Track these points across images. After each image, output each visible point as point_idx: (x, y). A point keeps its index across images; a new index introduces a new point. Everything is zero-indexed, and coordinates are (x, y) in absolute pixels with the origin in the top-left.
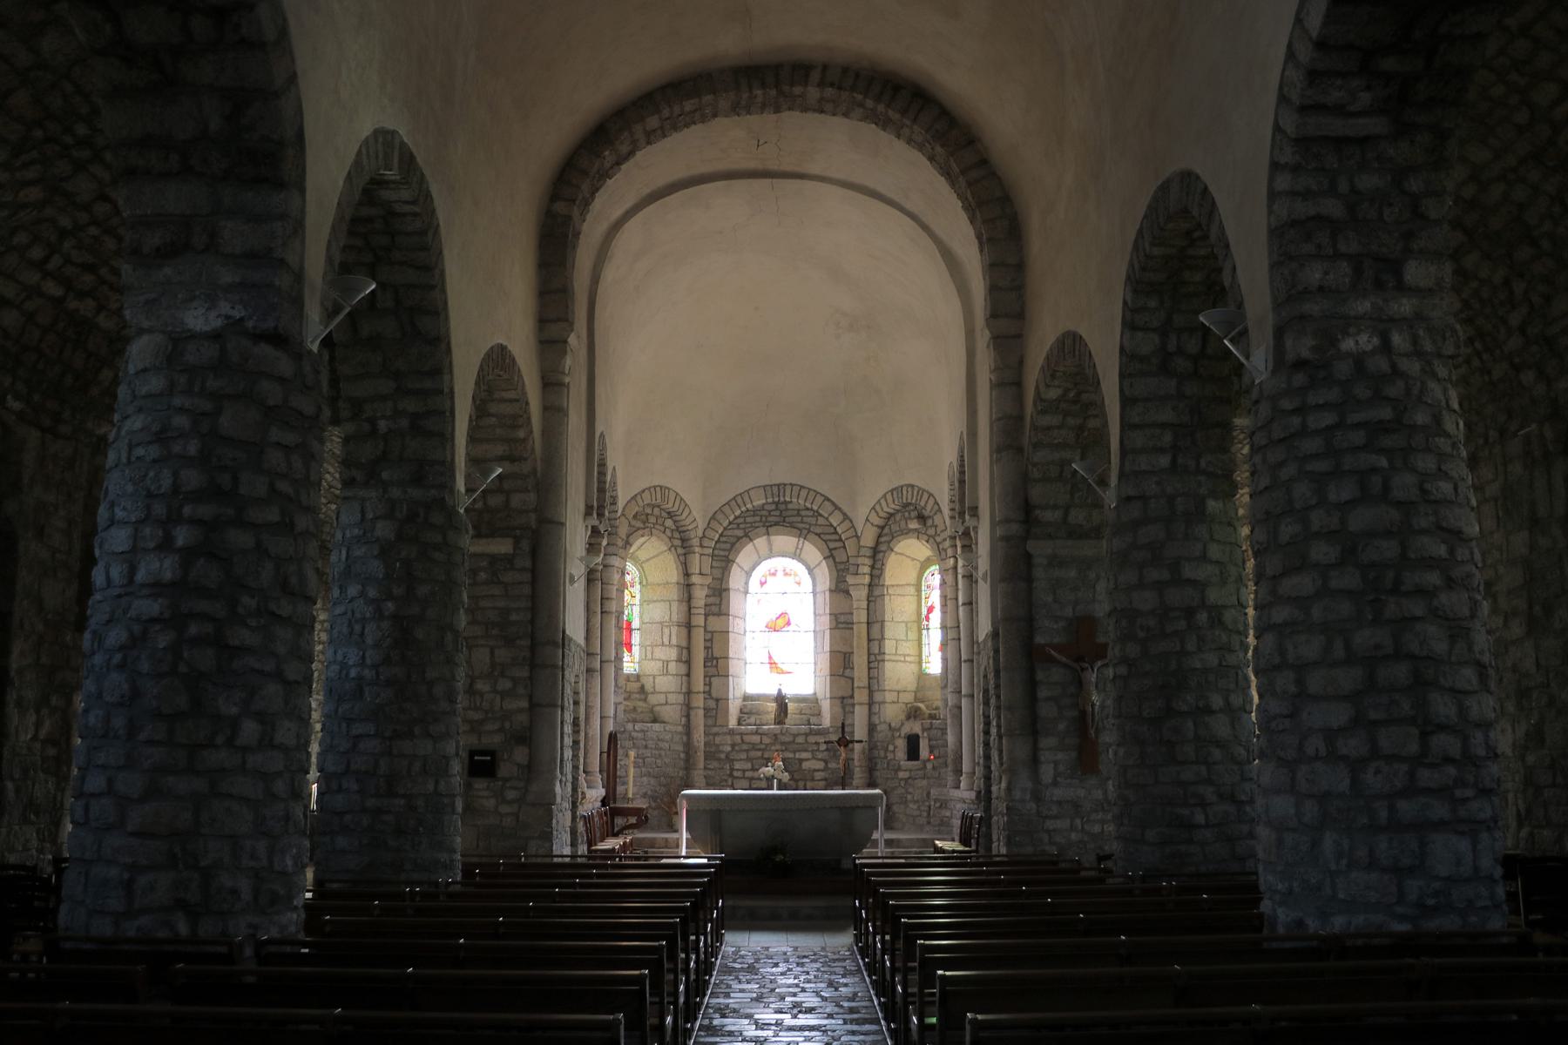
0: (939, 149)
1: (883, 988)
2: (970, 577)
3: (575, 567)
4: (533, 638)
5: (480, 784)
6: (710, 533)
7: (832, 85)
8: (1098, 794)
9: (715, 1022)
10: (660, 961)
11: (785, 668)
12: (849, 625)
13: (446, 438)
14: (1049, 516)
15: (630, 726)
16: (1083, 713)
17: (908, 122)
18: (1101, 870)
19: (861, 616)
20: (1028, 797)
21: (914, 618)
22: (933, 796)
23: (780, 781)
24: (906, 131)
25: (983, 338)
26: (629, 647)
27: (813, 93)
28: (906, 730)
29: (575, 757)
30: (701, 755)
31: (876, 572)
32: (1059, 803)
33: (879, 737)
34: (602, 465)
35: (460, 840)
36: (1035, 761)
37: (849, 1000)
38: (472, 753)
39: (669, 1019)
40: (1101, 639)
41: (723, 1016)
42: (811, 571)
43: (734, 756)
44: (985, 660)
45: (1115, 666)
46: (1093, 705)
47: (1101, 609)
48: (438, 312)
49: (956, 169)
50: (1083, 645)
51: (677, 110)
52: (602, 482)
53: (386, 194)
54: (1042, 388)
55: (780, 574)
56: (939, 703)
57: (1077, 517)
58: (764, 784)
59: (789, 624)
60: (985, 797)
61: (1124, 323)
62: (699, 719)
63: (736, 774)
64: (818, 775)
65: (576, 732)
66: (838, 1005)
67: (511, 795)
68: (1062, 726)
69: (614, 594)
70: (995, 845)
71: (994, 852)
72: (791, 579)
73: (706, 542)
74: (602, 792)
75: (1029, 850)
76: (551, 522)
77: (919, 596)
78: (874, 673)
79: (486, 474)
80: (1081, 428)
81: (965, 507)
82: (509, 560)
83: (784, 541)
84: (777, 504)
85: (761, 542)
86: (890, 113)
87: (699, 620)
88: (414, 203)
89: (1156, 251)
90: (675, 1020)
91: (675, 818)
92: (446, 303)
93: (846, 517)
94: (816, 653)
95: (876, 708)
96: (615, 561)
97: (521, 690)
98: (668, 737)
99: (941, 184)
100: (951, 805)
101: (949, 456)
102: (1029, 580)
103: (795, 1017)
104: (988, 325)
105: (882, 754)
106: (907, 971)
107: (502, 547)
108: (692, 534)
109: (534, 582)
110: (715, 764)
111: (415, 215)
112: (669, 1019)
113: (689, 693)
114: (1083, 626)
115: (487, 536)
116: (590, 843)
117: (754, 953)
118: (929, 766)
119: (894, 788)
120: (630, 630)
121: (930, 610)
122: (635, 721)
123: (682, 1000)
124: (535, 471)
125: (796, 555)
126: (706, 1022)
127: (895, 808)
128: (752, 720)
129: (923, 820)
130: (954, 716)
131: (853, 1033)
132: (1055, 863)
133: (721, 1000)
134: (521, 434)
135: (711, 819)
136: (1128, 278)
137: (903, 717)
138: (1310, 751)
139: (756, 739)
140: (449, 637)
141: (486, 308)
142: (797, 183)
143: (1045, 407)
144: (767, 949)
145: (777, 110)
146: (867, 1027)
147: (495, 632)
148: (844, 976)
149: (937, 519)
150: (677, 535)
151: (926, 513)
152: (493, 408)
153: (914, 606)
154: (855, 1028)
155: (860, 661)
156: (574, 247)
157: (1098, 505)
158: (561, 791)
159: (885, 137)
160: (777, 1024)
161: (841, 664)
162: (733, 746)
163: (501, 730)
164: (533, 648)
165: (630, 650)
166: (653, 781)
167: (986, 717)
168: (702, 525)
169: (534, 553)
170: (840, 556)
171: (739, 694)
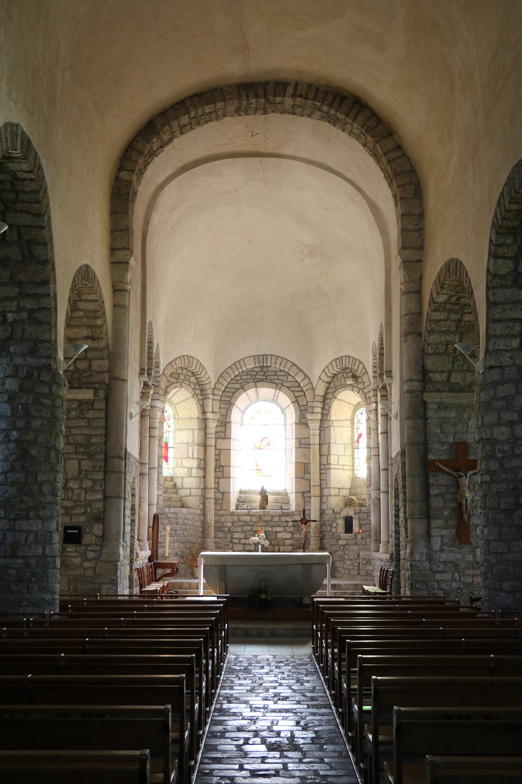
0: (369, 139)
1: (333, 684)
2: (386, 416)
3: (133, 407)
4: (106, 453)
5: (71, 548)
6: (219, 386)
7: (301, 96)
8: (470, 557)
9: (225, 706)
10: (192, 668)
12: (307, 446)
13: (51, 325)
14: (438, 377)
15: (167, 510)
16: (460, 504)
17: (350, 121)
18: (472, 608)
20: (424, 558)
21: (349, 441)
22: (361, 557)
23: (263, 546)
24: (349, 127)
25: (396, 261)
26: (166, 459)
27: (289, 101)
29: (132, 530)
30: (212, 529)
31: (325, 412)
32: (444, 562)
33: (326, 518)
34: (151, 342)
35: (58, 585)
36: (428, 536)
37: (311, 691)
38: (66, 528)
39: (197, 706)
40: (472, 457)
41: (230, 702)
42: (283, 410)
43: (234, 529)
44: (396, 470)
45: (482, 475)
46: (466, 500)
47: (472, 437)
48: (46, 243)
49: (381, 152)
50: (460, 461)
51: (200, 112)
52: (150, 353)
53: (12, 166)
54: (435, 295)
56: (365, 496)
57: (457, 378)
58: (253, 548)
59: (268, 444)
60: (396, 558)
61: (490, 254)
62: (211, 506)
63: (234, 541)
64: (288, 542)
65: (133, 514)
66: (304, 695)
67: (91, 555)
68: (446, 513)
69: (157, 425)
70: (402, 589)
71: (402, 594)
74: (148, 553)
75: (425, 593)
76: (118, 379)
77: (353, 427)
79: (77, 348)
80: (460, 321)
81: (383, 371)
82: (91, 403)
83: (266, 391)
84: (262, 367)
85: (251, 392)
86: (339, 115)
87: (211, 442)
88: (30, 172)
89: (513, 207)
90: (200, 706)
91: (195, 569)
92: (51, 237)
93: (306, 376)
95: (324, 499)
96: (158, 404)
97: (98, 488)
98: (191, 517)
99: (371, 161)
100: (373, 562)
101: (373, 338)
102: (425, 418)
103: (276, 703)
104: (400, 254)
105: (329, 528)
106: (349, 673)
107: (87, 395)
108: (208, 387)
109: (106, 418)
110: (221, 535)
111: (32, 180)
112: (197, 706)
113: (205, 489)
114: (460, 448)
115: (76, 388)
116: (141, 586)
117: (248, 659)
118: (359, 537)
119: (336, 551)
120: (167, 447)
121: (360, 436)
122: (170, 507)
123: (204, 691)
124: (108, 346)
125: (274, 400)
126: (218, 706)
127: (337, 564)
128: (245, 506)
129: (355, 572)
130: (375, 505)
131: (314, 714)
132: (443, 603)
133: (228, 691)
134: (99, 322)
135: (220, 571)
136: (493, 224)
137: (342, 505)
139: (248, 518)
140: (53, 453)
141: (77, 241)
142: (276, 160)
143: (436, 307)
144: (256, 656)
145: (265, 113)
146: (323, 711)
148: (306, 675)
149: (365, 378)
150: (197, 387)
151: (358, 374)
152: (81, 305)
153: (350, 433)
154: (315, 711)
155: (314, 469)
156: (133, 201)
157: (471, 370)
158: (123, 553)
159: (334, 131)
160: (264, 708)
161: (303, 470)
162: (233, 523)
163: (85, 513)
164: (106, 460)
165: (167, 461)
166: (181, 545)
167: (397, 506)
168: (213, 380)
169: (107, 398)
170: (302, 401)
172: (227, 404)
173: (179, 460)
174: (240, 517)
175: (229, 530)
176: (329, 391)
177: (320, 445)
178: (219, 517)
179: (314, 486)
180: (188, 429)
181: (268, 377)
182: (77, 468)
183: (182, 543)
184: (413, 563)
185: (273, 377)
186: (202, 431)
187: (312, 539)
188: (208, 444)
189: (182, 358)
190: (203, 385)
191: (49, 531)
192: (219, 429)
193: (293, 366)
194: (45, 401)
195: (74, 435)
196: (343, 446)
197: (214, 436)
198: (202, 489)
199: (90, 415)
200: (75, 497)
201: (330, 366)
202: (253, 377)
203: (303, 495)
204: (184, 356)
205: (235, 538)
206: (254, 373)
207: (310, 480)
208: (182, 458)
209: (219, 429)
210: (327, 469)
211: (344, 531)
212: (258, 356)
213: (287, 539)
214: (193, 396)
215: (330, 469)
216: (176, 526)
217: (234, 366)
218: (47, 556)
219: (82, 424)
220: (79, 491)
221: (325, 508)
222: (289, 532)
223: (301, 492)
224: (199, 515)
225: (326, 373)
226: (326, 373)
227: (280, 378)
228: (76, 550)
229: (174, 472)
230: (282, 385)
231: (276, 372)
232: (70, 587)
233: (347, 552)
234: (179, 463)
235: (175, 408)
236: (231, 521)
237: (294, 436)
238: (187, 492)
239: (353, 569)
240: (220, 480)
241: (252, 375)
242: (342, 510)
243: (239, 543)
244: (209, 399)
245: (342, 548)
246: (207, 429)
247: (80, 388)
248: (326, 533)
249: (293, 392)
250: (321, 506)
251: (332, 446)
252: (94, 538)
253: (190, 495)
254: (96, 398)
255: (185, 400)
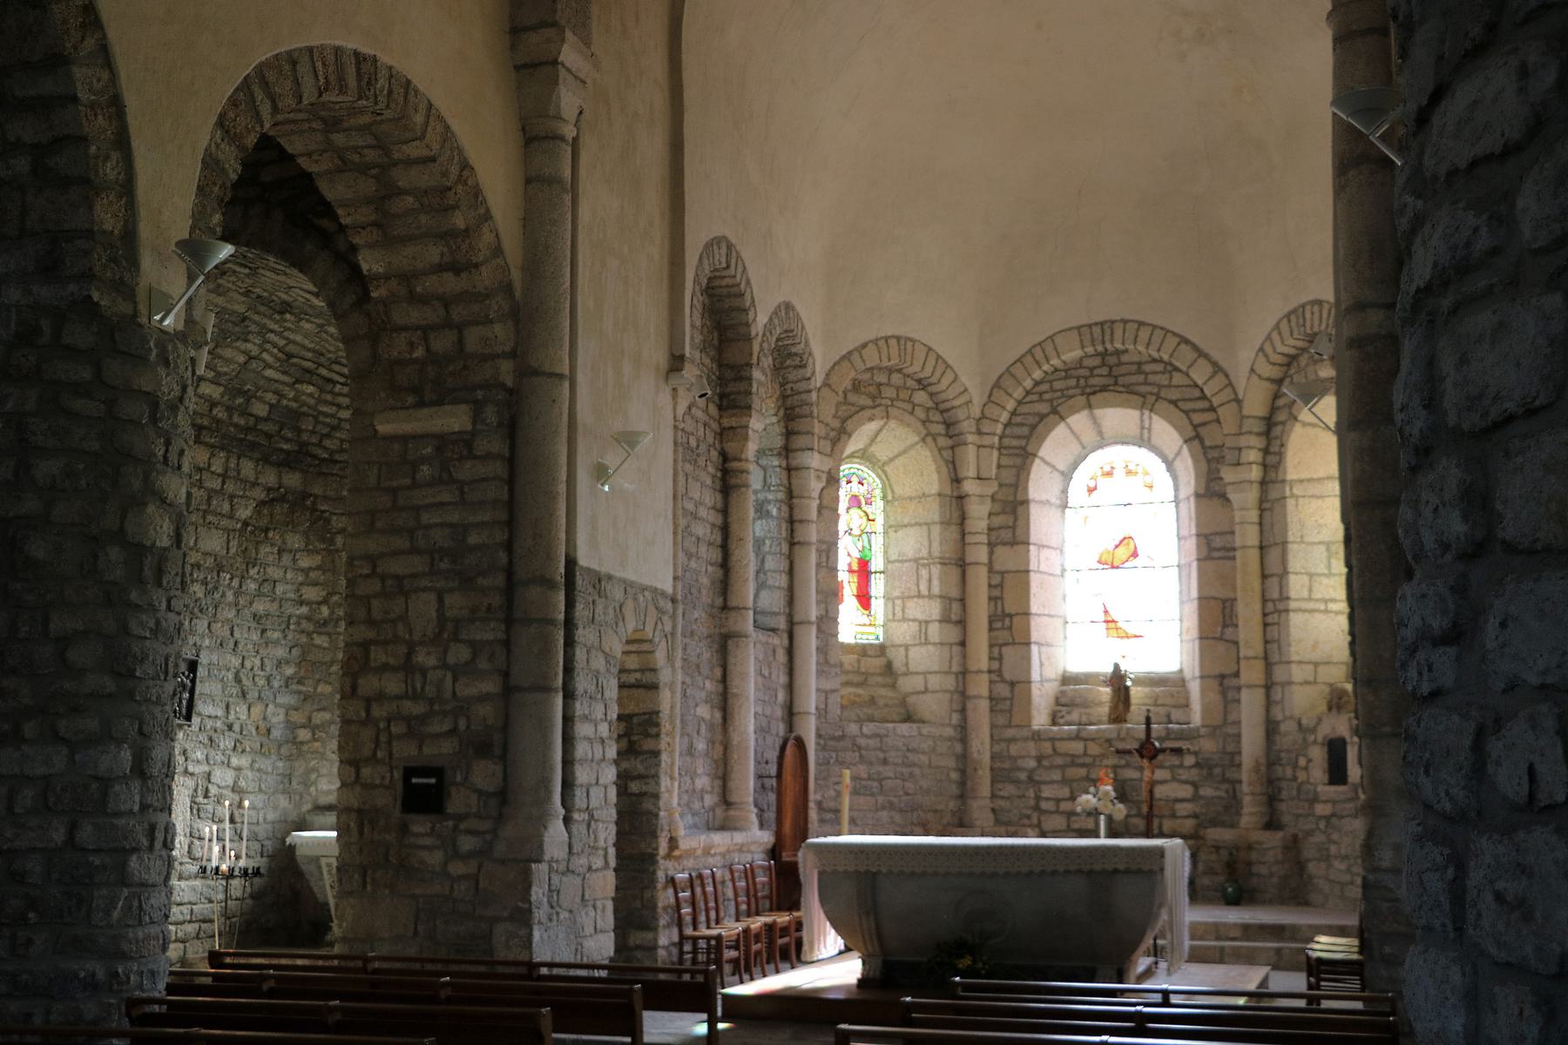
5: (420, 825)
6: (993, 411)
11: (1131, 631)
12: (1229, 553)
19: (1248, 536)
23: (1110, 819)
28: (1325, 731)
30: (984, 776)
31: (1271, 459)
38: (409, 773)
55: (1119, 472)
59: (1135, 554)
62: (981, 714)
63: (1044, 805)
64: (1183, 809)
67: (467, 843)
72: (1137, 481)
73: (986, 427)
76: (537, 373)
78: (1273, 632)
82: (464, 443)
83: (1118, 417)
85: (1079, 420)
87: (979, 554)
93: (1217, 368)
94: (1182, 603)
95: (1277, 694)
97: (483, 664)
98: (925, 746)
105: (1289, 772)
107: (454, 419)
108: (961, 414)
110: (1009, 790)
115: (432, 404)
119: (1309, 833)
124: (508, 288)
125: (1143, 440)
128: (1075, 716)
138: (1509, 780)
139: (1077, 747)
147: (444, 565)
150: (937, 417)
155: (1248, 614)
161: (1216, 618)
162: (1039, 759)
163: (453, 731)
168: (978, 398)
171: (1053, 672)
172: (1019, 454)
173: (898, 602)
174: (1058, 744)
175: (1030, 778)
176: (1281, 402)
177: (1261, 548)
178: (1003, 745)
179: (1247, 658)
180: (917, 524)
181: (1121, 380)
182: (434, 615)
183: (901, 811)
184: (1370, 877)
185: (1134, 379)
186: (954, 528)
187: (1247, 800)
188: (969, 559)
189: (882, 343)
190: (947, 410)
191: (96, 778)
192: (997, 521)
193: (1183, 346)
194: (79, 404)
195: (429, 527)
196: (1323, 548)
197: (984, 539)
198: (957, 674)
199: (466, 471)
200: (430, 691)
201: (1275, 336)
202: (1082, 381)
203: (1221, 684)
204: (886, 339)
205: (1048, 799)
206: (1082, 372)
207: (1236, 643)
208: (903, 598)
209: (997, 521)
210: (1280, 612)
211: (1326, 779)
212: (1090, 326)
213: (1182, 800)
214: (923, 440)
215: (1287, 611)
216: (881, 769)
217: (1029, 358)
218: (83, 850)
219: (446, 497)
220: (439, 673)
221: (1280, 717)
222: (1186, 782)
223: (1215, 677)
224: (950, 739)
225: (1266, 356)
226: (1266, 356)
227: (1151, 378)
228: (433, 829)
229: (885, 632)
230: (1158, 397)
231: (1139, 364)
232: (419, 928)
233: (1335, 836)
234: (898, 609)
235: (885, 472)
236: (1034, 753)
237: (1194, 531)
238: (916, 683)
239: (1352, 883)
240: (1004, 649)
241: (1078, 378)
242: (1320, 720)
243: (1057, 812)
244: (965, 444)
245: (1322, 825)
246: (967, 522)
247: (439, 403)
248: (1284, 784)
249: (1186, 413)
250: (1268, 711)
251: (1292, 548)
252: (474, 797)
253: (926, 690)
254: (479, 427)
255: (905, 452)
